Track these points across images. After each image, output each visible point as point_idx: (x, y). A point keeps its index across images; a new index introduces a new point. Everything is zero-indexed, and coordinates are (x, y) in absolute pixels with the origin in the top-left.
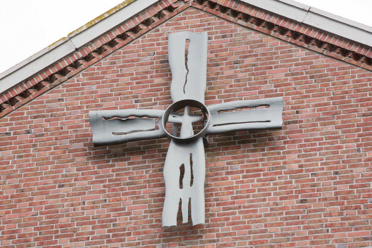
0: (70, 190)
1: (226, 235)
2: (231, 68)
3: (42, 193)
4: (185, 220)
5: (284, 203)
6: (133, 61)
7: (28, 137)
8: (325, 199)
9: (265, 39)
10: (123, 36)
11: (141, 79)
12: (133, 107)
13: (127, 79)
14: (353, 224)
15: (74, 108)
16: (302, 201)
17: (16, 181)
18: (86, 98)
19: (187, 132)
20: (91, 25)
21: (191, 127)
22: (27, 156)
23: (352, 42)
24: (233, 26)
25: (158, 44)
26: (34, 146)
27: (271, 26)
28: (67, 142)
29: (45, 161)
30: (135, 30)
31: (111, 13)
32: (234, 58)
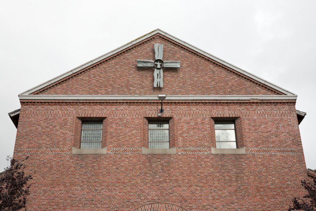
0: (132, 76)
1: (167, 90)
2: (167, 53)
3: (125, 76)
4: (159, 86)
5: (180, 84)
6: (145, 49)
7: (122, 63)
8: (188, 84)
9: (175, 47)
10: (143, 43)
11: (147, 53)
12: (146, 59)
13: (144, 53)
14: (194, 90)
15: (132, 58)
16: (183, 84)
17: (120, 73)
18: (135, 56)
19: (159, 66)
20: (136, 40)
21: (160, 65)
22: (122, 68)
23: (194, 51)
24: (168, 44)
25: (151, 46)
26: (124, 65)
27: (176, 45)
28: (131, 66)
29: (126, 69)
30: (146, 42)
31: (141, 37)
32: (168, 51)
